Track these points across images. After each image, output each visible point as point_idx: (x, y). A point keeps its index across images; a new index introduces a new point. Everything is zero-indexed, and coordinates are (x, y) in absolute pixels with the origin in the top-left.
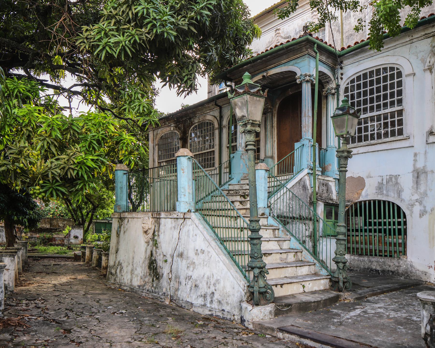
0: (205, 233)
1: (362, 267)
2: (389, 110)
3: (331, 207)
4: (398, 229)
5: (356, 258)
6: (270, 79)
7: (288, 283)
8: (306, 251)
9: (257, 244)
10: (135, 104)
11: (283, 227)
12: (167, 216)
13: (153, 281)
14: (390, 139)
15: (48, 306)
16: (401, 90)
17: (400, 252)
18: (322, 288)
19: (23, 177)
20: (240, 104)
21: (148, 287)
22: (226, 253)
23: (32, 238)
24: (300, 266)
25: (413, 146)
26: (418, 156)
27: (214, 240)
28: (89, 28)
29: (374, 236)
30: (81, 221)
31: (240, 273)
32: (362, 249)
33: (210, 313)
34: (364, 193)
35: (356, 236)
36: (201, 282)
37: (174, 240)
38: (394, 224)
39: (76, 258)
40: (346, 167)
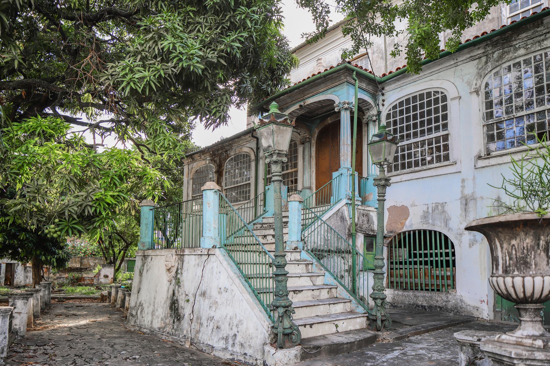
0: (229, 270)
1: (407, 303)
2: (434, 135)
3: (372, 238)
4: (446, 260)
5: (400, 293)
6: (308, 108)
7: (318, 323)
8: (341, 287)
9: (282, 281)
10: (160, 139)
11: (317, 261)
12: (191, 252)
13: (174, 321)
14: (435, 165)
15: (57, 352)
16: (447, 114)
17: (448, 285)
18: (358, 327)
19: (38, 216)
20: (265, 134)
21: (168, 329)
22: (251, 291)
23: (60, 278)
24: (334, 304)
25: (460, 172)
26: (466, 182)
27: (238, 277)
28: (114, 65)
29: (420, 269)
30: (112, 260)
31: (265, 312)
32: (406, 283)
33: (231, 357)
34: (408, 222)
35: (400, 269)
36: (223, 323)
37: (197, 277)
38: (441, 256)
39: (103, 298)
40: (384, 196)
